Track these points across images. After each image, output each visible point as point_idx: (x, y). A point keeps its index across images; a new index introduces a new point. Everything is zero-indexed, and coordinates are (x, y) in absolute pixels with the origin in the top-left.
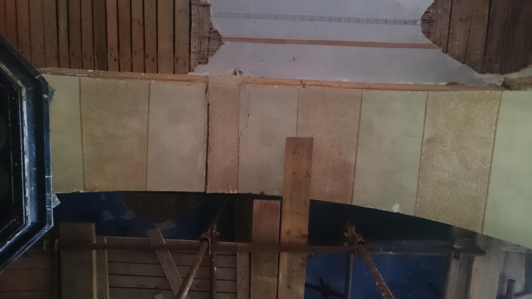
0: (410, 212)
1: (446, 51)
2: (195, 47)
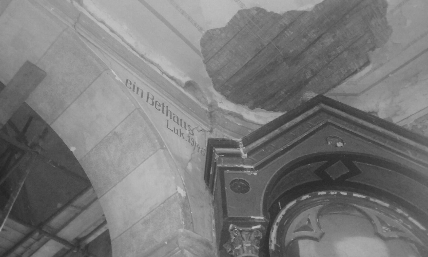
1: (205, 62)
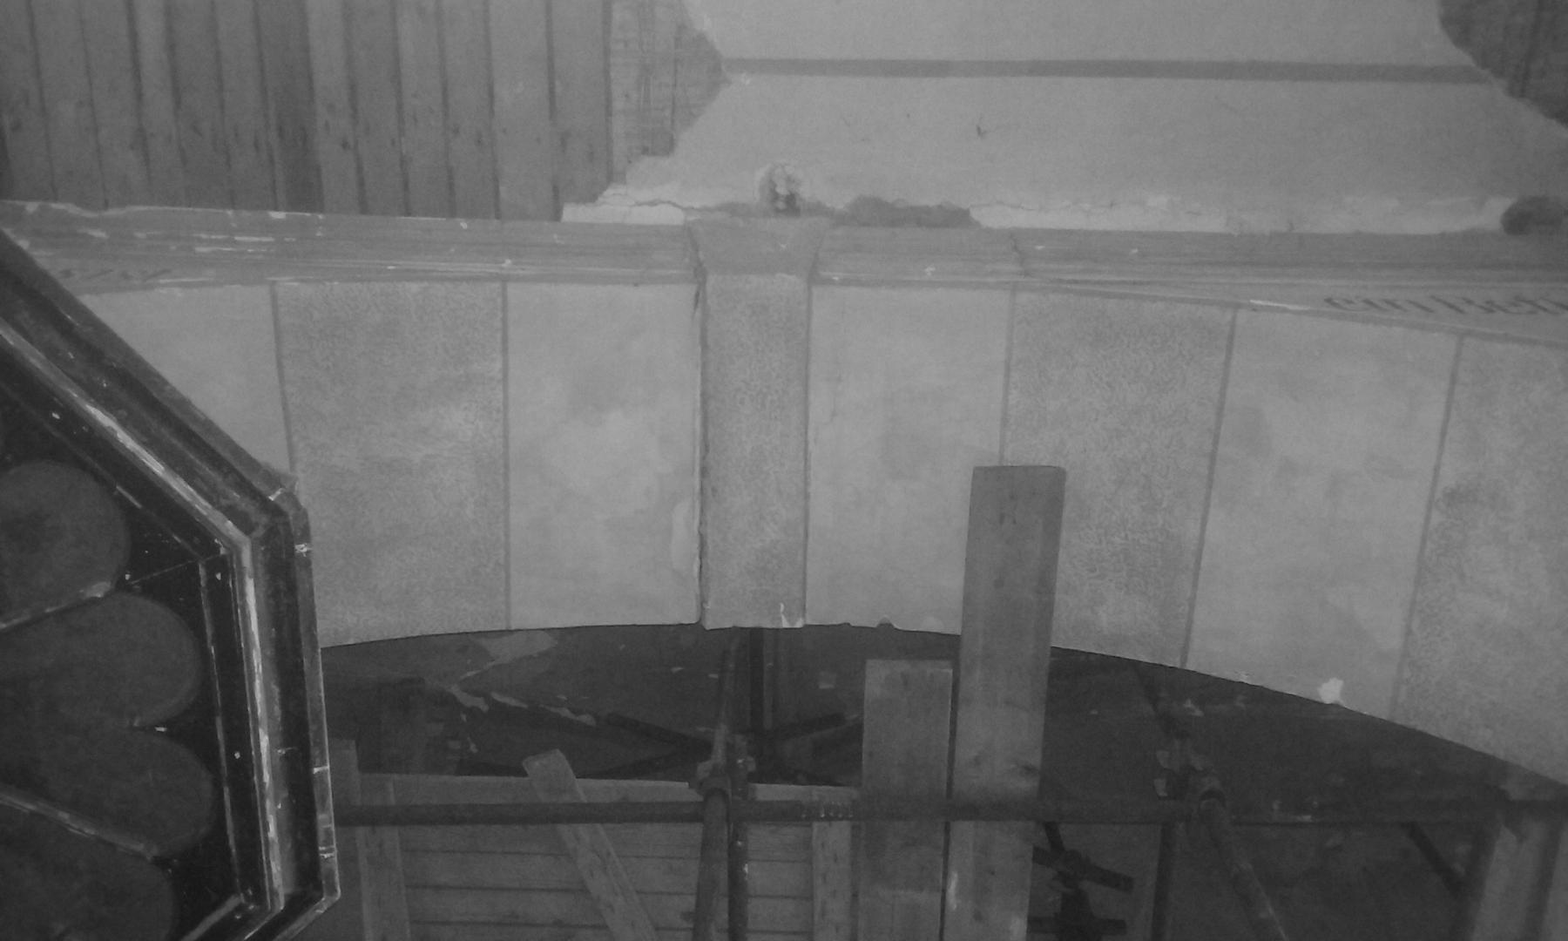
0: (1377, 707)
2: (627, 96)
